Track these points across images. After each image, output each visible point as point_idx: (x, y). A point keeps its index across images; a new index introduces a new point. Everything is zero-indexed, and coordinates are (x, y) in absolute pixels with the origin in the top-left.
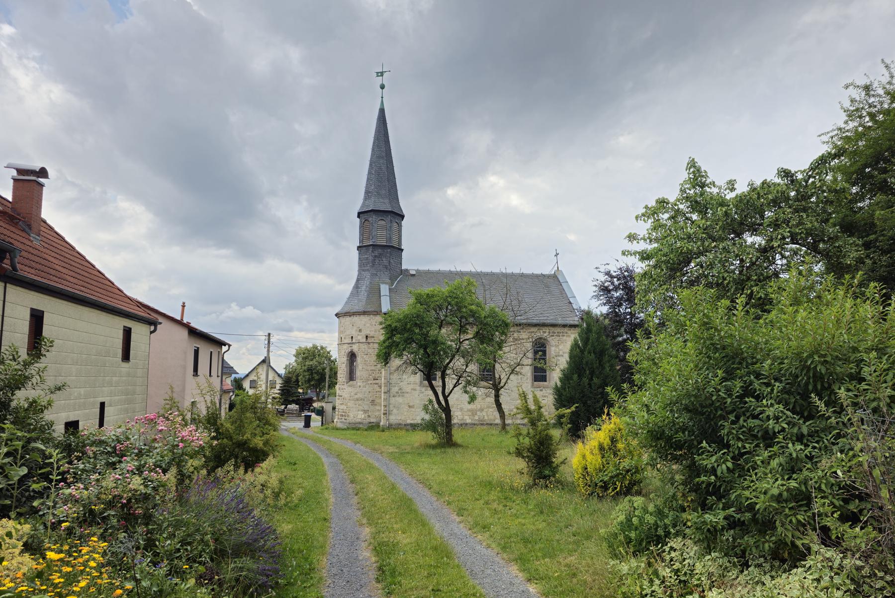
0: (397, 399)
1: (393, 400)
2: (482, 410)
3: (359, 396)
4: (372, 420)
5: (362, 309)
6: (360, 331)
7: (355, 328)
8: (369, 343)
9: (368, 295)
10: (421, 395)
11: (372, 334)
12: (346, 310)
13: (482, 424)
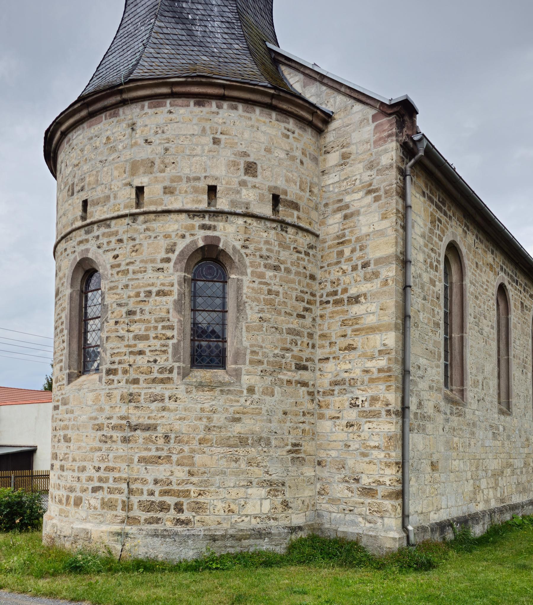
3: (248, 426)
4: (298, 520)
7: (226, 154)
8: (284, 225)
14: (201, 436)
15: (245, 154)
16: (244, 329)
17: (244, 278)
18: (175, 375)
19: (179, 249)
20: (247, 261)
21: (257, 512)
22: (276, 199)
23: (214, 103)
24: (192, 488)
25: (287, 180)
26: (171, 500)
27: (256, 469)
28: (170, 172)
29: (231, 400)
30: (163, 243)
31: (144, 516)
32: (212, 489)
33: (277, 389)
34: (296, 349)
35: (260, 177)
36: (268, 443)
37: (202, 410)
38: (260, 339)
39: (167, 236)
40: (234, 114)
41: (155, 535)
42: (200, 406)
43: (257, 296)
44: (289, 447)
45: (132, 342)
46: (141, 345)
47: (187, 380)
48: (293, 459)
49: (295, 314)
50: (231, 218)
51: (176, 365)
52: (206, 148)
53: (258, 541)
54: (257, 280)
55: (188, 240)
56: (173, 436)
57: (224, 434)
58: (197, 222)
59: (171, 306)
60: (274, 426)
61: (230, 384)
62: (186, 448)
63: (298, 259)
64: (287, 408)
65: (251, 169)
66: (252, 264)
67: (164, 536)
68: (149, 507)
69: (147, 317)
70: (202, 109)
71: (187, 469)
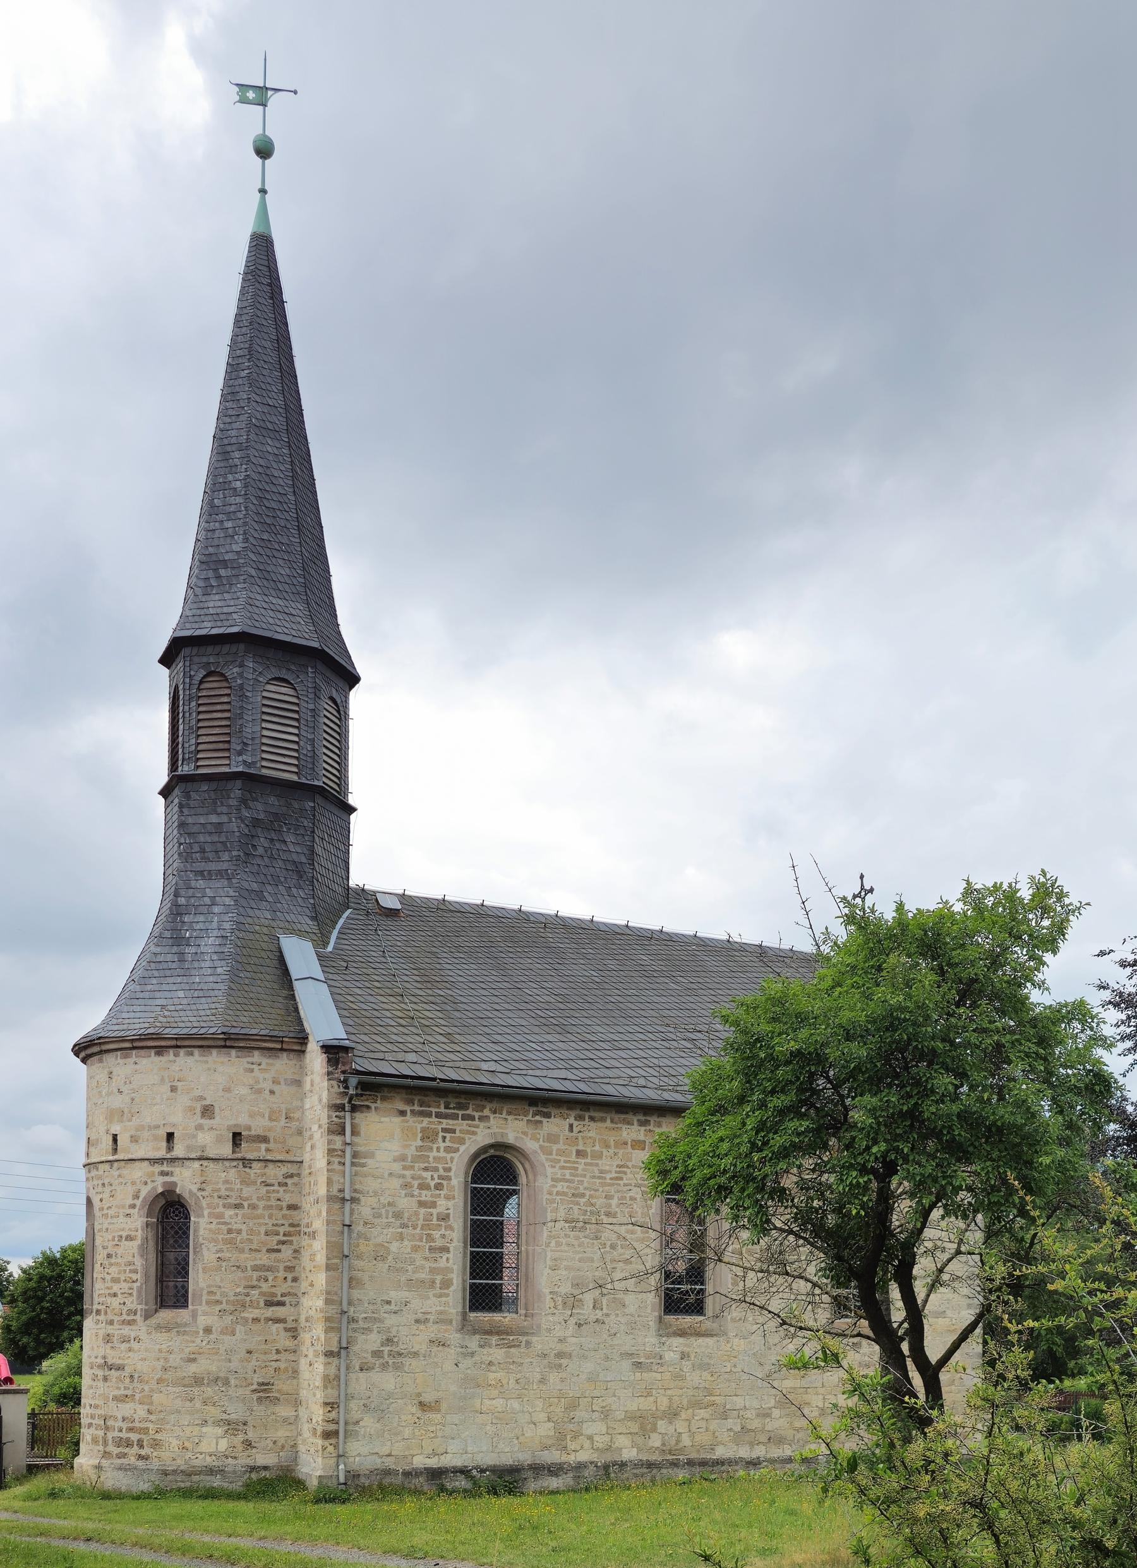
0: (375, 1376)
1: (360, 1383)
2: (672, 1415)
4: (262, 1460)
5: (214, 1028)
6: (208, 1111)
7: (184, 1100)
8: (246, 1162)
9: (233, 975)
10: (467, 1362)
11: (258, 1126)
12: (137, 1024)
13: (674, 1464)
14: (158, 1376)
15: (202, 1098)
16: (201, 1270)
17: (201, 1220)
18: (138, 1317)
19: (143, 1195)
20: (204, 1203)
21: (212, 1449)
22: (237, 1137)
23: (171, 1051)
24: (151, 1426)
25: (252, 1115)
26: (134, 1437)
27: (212, 1409)
28: (136, 1121)
29: (187, 1341)
30: (130, 1190)
31: (116, 1451)
32: (168, 1427)
33: (239, 1328)
34: (265, 1287)
35: (217, 1118)
36: (226, 1382)
37: (160, 1351)
38: (218, 1279)
39: (133, 1183)
40: (190, 1060)
41: (120, 1468)
42: (158, 1346)
43: (214, 1236)
44: (255, 1387)
45: (110, 1284)
46: (116, 1288)
47: (148, 1322)
48: (259, 1399)
49: (264, 1250)
50: (187, 1163)
51: (140, 1307)
52: (165, 1096)
53: (208, 1478)
54: (215, 1221)
55: (150, 1186)
56: (136, 1376)
57: (180, 1374)
58: (157, 1168)
59: (135, 1250)
60: (234, 1365)
61: (186, 1325)
62: (146, 1388)
63: (268, 1192)
64: (251, 1347)
65: (208, 1111)
66: (209, 1206)
67: (126, 1470)
68: (119, 1442)
69: (119, 1260)
70: (161, 1058)
71: (146, 1407)
